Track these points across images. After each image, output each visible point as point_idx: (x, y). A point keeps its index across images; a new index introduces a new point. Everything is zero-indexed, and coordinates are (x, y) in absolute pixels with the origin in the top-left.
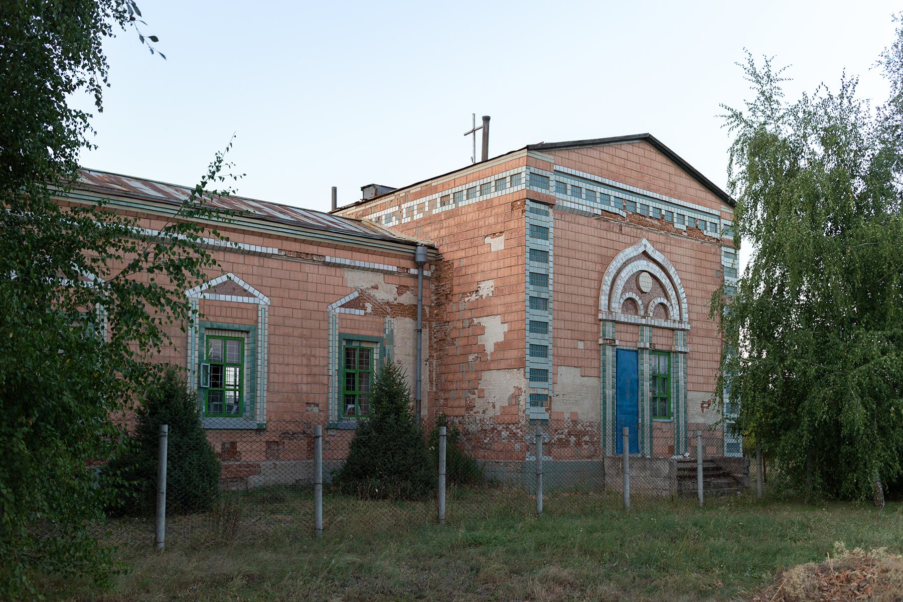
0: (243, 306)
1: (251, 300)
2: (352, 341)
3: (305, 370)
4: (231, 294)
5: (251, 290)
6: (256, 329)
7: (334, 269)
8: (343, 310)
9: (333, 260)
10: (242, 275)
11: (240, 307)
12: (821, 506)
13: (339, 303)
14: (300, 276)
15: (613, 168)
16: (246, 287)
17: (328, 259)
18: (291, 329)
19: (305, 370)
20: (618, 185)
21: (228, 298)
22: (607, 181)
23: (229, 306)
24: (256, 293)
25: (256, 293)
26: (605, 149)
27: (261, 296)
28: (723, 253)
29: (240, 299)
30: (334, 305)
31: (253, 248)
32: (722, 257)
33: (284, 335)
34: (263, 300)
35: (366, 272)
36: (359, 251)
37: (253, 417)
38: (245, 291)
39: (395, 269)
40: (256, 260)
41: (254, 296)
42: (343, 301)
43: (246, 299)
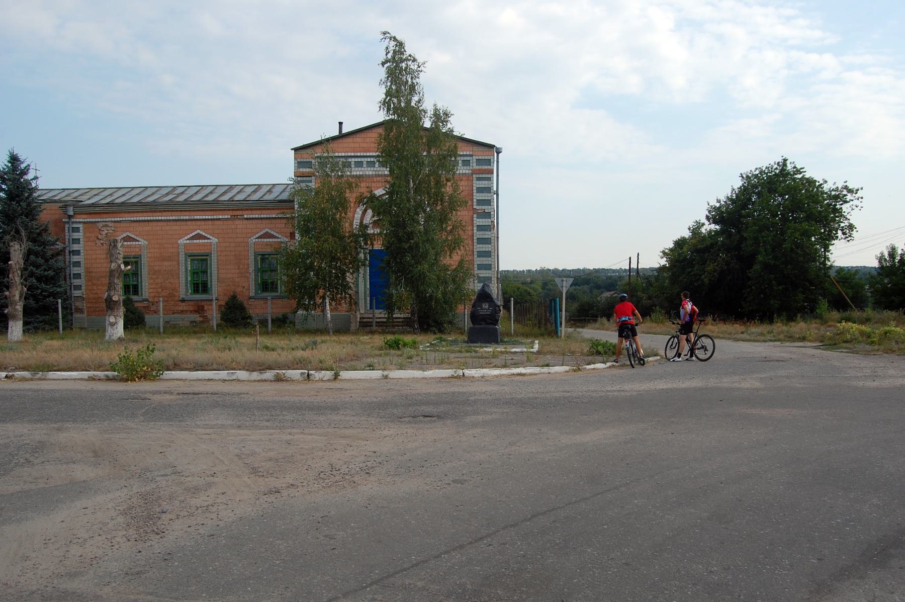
0: (130, 246)
1: (209, 241)
2: (265, 255)
3: (237, 271)
4: (199, 239)
5: (208, 236)
6: (211, 254)
7: (194, 222)
8: (257, 240)
9: (249, 217)
10: (204, 230)
11: (203, 244)
12: (265, 336)
13: (255, 237)
14: (233, 227)
15: (365, 145)
16: (206, 235)
17: (245, 216)
18: (229, 252)
19: (237, 271)
20: (368, 154)
21: (198, 241)
22: (359, 154)
23: (199, 244)
24: (211, 237)
25: (211, 237)
26: (358, 135)
27: (214, 238)
28: (475, 179)
29: (203, 241)
30: (252, 238)
31: (207, 217)
32: (474, 182)
33: (226, 255)
34: (214, 240)
35: (248, 220)
36: (264, 209)
37: (142, 295)
38: (131, 238)
39: (229, 217)
40: (210, 222)
41: (257, 238)
42: (257, 236)
43: (206, 241)
